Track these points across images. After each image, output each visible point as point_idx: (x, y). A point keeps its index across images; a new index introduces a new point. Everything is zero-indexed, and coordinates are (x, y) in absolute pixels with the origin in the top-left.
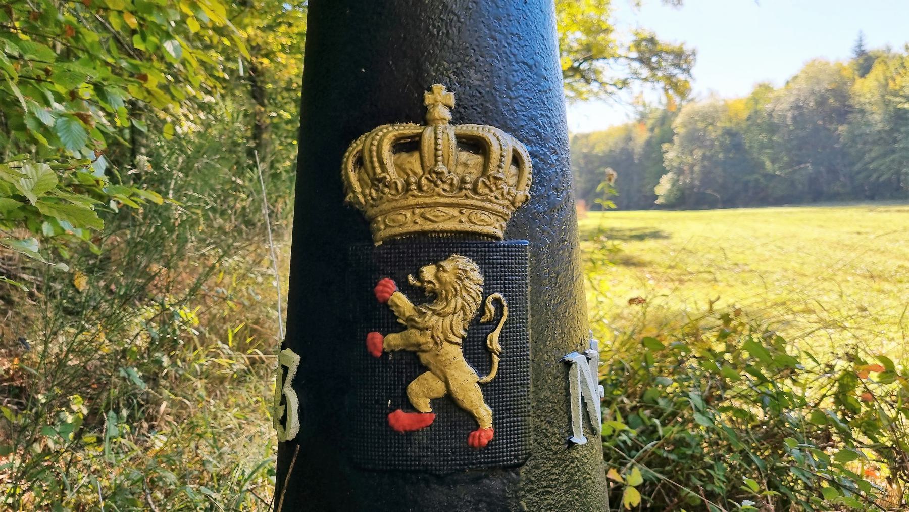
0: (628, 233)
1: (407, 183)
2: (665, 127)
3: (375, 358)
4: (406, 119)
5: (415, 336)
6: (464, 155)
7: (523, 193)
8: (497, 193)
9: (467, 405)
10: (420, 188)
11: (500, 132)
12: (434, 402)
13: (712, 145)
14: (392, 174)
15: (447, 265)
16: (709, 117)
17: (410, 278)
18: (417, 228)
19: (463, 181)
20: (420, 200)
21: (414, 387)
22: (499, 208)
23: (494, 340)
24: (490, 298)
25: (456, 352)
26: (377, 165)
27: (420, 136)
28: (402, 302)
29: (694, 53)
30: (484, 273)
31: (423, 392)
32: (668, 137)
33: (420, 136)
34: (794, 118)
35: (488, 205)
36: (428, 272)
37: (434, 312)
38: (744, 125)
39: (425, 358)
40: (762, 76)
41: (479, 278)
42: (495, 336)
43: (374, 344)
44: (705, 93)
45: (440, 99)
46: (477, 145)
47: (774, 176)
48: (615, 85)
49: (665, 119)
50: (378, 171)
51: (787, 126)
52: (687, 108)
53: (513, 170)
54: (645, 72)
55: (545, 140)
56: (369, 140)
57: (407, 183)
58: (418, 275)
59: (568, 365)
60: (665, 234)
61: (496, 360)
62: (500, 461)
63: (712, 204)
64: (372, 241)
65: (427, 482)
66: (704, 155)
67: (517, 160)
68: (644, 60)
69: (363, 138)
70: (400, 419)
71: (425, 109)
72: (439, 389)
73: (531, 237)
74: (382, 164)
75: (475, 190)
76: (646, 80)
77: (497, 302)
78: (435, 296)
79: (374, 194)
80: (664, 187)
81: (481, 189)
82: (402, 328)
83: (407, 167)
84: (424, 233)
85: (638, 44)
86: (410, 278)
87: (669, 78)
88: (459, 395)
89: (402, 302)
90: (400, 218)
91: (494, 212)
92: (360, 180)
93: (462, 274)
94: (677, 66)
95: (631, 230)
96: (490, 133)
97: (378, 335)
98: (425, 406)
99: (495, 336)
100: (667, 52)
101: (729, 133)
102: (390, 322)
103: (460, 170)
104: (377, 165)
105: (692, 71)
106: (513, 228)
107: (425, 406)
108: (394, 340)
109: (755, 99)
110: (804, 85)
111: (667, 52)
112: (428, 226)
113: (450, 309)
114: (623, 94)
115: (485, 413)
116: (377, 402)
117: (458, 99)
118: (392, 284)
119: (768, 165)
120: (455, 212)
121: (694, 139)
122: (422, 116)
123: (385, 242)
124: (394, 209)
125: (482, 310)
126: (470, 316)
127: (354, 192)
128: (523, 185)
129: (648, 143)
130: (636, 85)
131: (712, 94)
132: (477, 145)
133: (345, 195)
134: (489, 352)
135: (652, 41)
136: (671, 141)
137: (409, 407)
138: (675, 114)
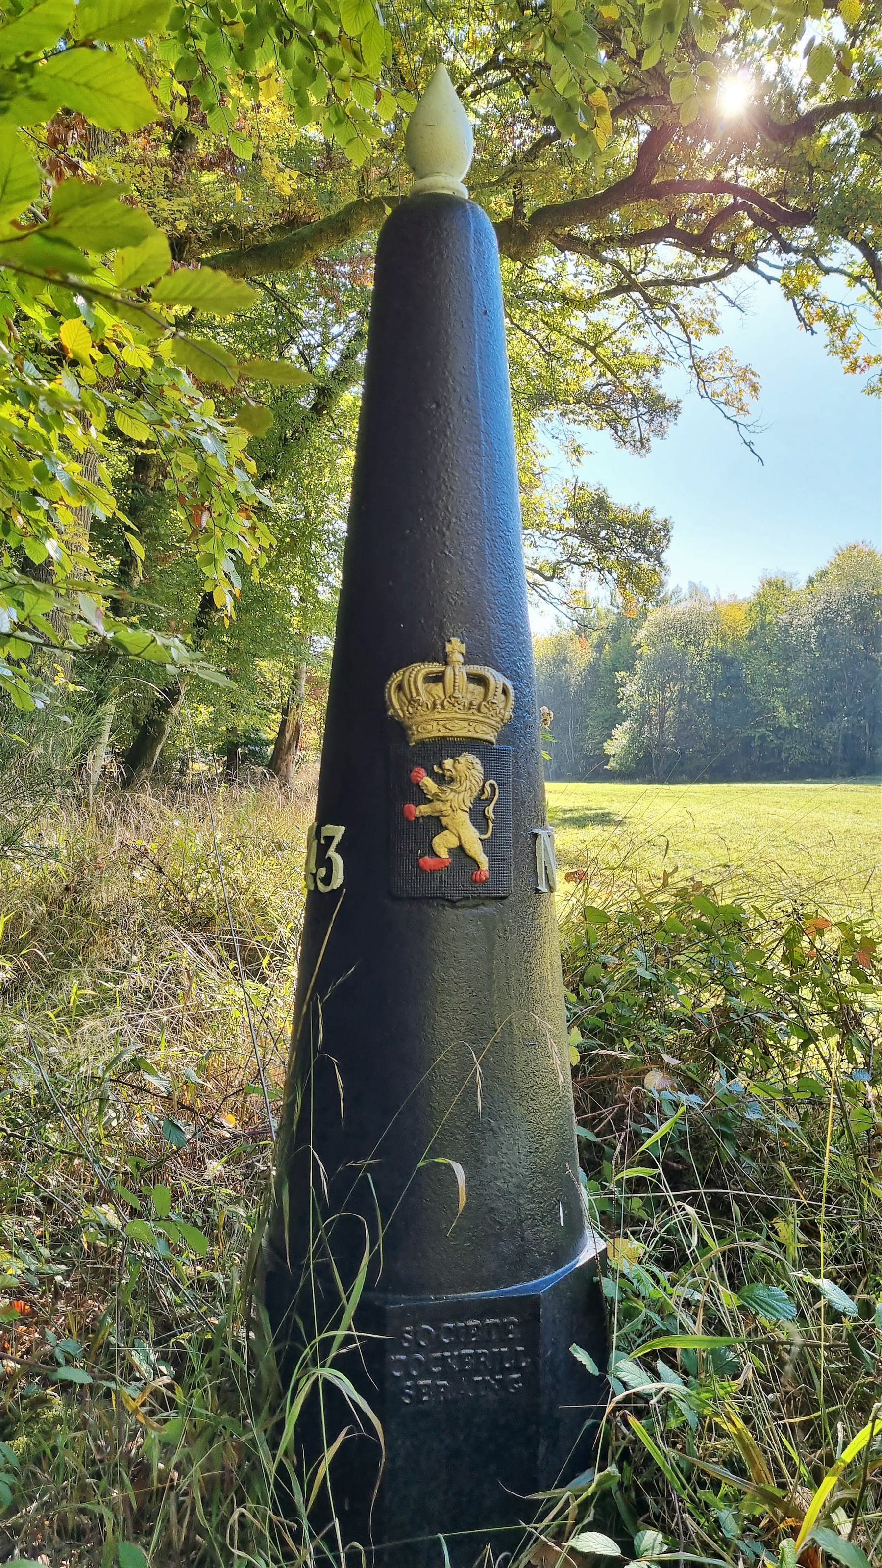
0: (560, 815)
1: (434, 704)
2: (620, 644)
3: (409, 821)
4: (435, 660)
5: (439, 805)
6: (472, 686)
7: (508, 714)
8: (493, 713)
9: (472, 853)
10: (443, 707)
11: (494, 672)
12: (450, 851)
13: (694, 677)
14: (424, 698)
15: (461, 759)
16: (688, 631)
17: (435, 768)
18: (440, 734)
19: (471, 704)
20: (443, 716)
21: (437, 841)
22: (494, 723)
23: (490, 811)
24: (488, 783)
25: (464, 818)
26: (413, 690)
27: (444, 672)
28: (429, 784)
29: (666, 527)
30: (484, 766)
31: (443, 844)
32: (626, 660)
33: (444, 672)
34: (821, 638)
35: (487, 720)
36: (448, 763)
37: (452, 790)
38: (745, 646)
39: (445, 821)
40: (775, 567)
41: (482, 770)
42: (491, 808)
43: (411, 813)
44: (685, 590)
45: (456, 648)
46: (480, 680)
47: (789, 731)
48: (539, 572)
49: (618, 630)
50: (414, 695)
51: (811, 651)
52: (655, 614)
53: (503, 697)
54: (588, 553)
55: (522, 678)
56: (407, 674)
57: (434, 704)
58: (441, 766)
59: (536, 835)
60: (617, 819)
61: (491, 825)
62: (490, 894)
63: (695, 777)
64: (407, 743)
65: (443, 905)
66: (681, 691)
67: (505, 692)
68: (586, 535)
69: (401, 672)
70: (428, 861)
71: (446, 655)
72: (454, 843)
73: (513, 744)
74: (417, 689)
75: (479, 710)
76: (589, 565)
77: (492, 785)
78: (452, 780)
79: (411, 710)
80: (617, 744)
81: (484, 710)
82: (431, 801)
83: (434, 692)
84: (445, 738)
85: (574, 510)
86: (435, 768)
87: (627, 564)
88: (467, 846)
89: (429, 784)
90: (429, 727)
91: (490, 726)
92: (399, 699)
93: (468, 769)
94: (639, 547)
95: (565, 811)
96: (489, 672)
97: (412, 806)
98: (444, 854)
99: (491, 808)
100: (623, 524)
101: (718, 657)
102: (423, 798)
103: (469, 696)
104: (413, 690)
105: (664, 557)
106: (502, 737)
107: (444, 854)
108: (424, 809)
109: (761, 605)
110: (837, 589)
111: (623, 524)
112: (448, 734)
113: (463, 788)
114: (554, 587)
115: (483, 860)
116: (410, 851)
117: (467, 648)
118: (422, 771)
119: (782, 713)
120: (466, 724)
121: (668, 667)
122: (445, 660)
123: (417, 744)
124: (426, 721)
125: (482, 791)
126: (475, 794)
127: (394, 708)
128: (508, 709)
129: (592, 669)
130: (574, 574)
131: (695, 590)
132: (480, 680)
133: (386, 711)
134: (486, 819)
135: (600, 503)
136: (630, 668)
137: (434, 854)
138: (637, 624)
